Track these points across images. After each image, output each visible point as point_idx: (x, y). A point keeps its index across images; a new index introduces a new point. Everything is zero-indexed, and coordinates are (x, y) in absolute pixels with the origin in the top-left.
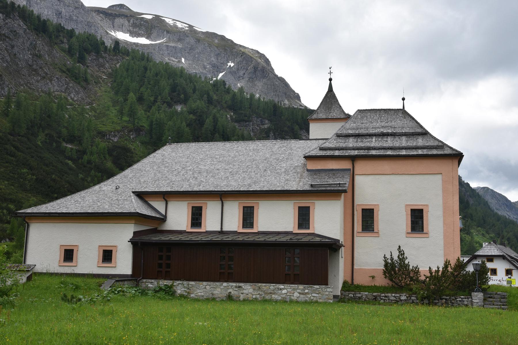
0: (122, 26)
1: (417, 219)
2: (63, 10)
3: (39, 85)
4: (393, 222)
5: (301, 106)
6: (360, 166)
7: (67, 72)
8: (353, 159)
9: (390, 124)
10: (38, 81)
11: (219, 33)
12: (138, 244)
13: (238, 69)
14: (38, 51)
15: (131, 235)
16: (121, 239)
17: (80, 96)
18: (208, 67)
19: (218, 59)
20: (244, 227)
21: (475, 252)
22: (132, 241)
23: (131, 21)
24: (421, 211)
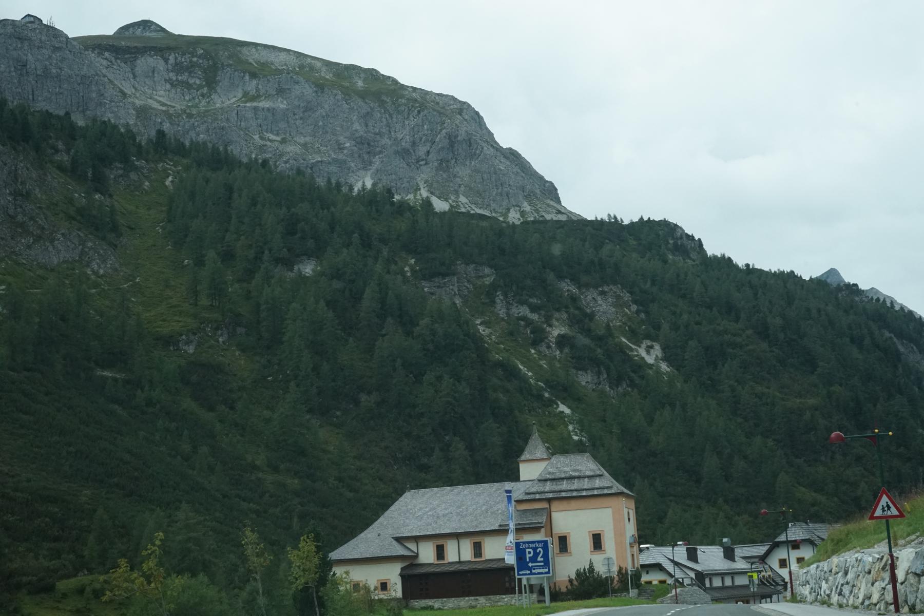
0: (153, 72)
1: (597, 542)
2: (30, 57)
3: (32, 253)
4: (580, 545)
5: (559, 212)
6: (555, 505)
7: (79, 218)
8: (549, 500)
9: (578, 468)
10: (29, 247)
11: (365, 65)
12: (405, 578)
13: (414, 144)
14: (22, 183)
15: (399, 571)
16: (392, 574)
17: (109, 266)
18: (348, 145)
19: (367, 126)
20: (475, 557)
21: (776, 537)
22: (400, 575)
23: (172, 59)
24: (599, 535)
